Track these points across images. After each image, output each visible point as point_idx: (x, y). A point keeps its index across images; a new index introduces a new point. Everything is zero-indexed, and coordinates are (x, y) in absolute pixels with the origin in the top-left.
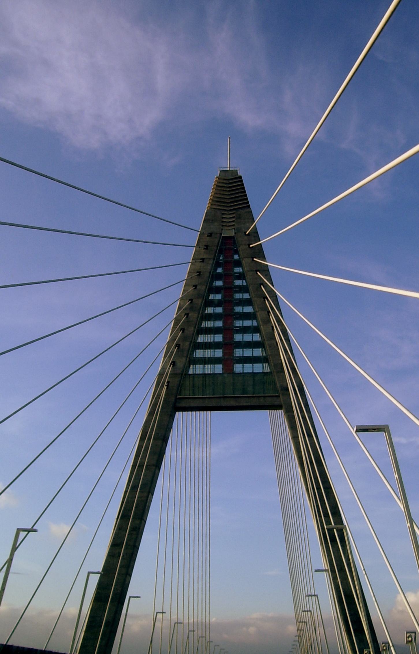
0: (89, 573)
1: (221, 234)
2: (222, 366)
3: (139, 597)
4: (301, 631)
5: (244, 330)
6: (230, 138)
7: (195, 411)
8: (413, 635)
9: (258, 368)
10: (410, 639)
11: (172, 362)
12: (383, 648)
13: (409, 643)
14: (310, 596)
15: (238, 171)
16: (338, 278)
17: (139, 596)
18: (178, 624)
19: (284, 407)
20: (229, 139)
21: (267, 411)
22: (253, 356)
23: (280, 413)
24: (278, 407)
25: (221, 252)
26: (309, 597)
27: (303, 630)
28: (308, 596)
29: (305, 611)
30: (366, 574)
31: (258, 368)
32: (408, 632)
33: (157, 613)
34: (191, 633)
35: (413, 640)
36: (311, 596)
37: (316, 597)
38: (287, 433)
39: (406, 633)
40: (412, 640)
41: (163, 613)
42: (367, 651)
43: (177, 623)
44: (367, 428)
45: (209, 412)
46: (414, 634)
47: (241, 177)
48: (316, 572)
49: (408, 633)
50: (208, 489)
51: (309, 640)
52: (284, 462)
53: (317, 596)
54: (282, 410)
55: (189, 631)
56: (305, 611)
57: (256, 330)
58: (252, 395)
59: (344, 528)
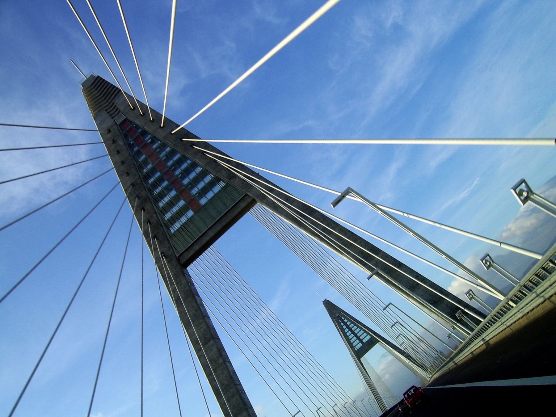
0: (390, 303)
1: (116, 124)
2: (184, 184)
3: (363, 399)
4: (403, 344)
5: (187, 172)
6: (71, 60)
7: (201, 254)
8: (471, 292)
9: (217, 189)
10: (488, 263)
11: (161, 254)
12: (470, 297)
13: (490, 267)
14: (386, 308)
15: (94, 75)
16: (171, 16)
17: (320, 407)
18: (317, 409)
19: (257, 199)
20: (71, 61)
21: (247, 213)
22: (211, 190)
23: (259, 207)
24: (252, 203)
25: (126, 136)
26: (386, 309)
27: (404, 342)
28: (385, 309)
29: (398, 337)
30: (408, 214)
31: (217, 189)
32: (514, 188)
33: (344, 405)
34: (335, 408)
35: (473, 295)
36: (394, 325)
37: (397, 323)
38: (273, 214)
39: (481, 261)
40: (490, 263)
41: (346, 403)
42: (458, 314)
43: (319, 409)
44: (338, 199)
45: (211, 246)
46: (488, 257)
47: (98, 77)
48: (370, 279)
49: (483, 260)
50: (260, 301)
51: (417, 357)
52: (322, 274)
53: (390, 303)
54: (258, 203)
55: (333, 407)
56: (398, 337)
57: (194, 166)
58: (228, 210)
59: (377, 271)
